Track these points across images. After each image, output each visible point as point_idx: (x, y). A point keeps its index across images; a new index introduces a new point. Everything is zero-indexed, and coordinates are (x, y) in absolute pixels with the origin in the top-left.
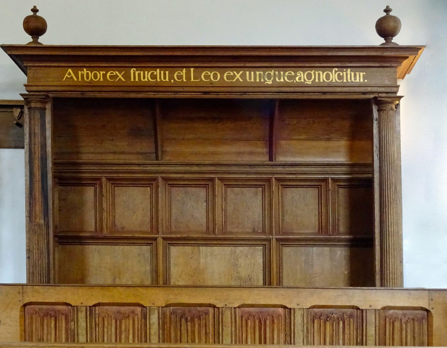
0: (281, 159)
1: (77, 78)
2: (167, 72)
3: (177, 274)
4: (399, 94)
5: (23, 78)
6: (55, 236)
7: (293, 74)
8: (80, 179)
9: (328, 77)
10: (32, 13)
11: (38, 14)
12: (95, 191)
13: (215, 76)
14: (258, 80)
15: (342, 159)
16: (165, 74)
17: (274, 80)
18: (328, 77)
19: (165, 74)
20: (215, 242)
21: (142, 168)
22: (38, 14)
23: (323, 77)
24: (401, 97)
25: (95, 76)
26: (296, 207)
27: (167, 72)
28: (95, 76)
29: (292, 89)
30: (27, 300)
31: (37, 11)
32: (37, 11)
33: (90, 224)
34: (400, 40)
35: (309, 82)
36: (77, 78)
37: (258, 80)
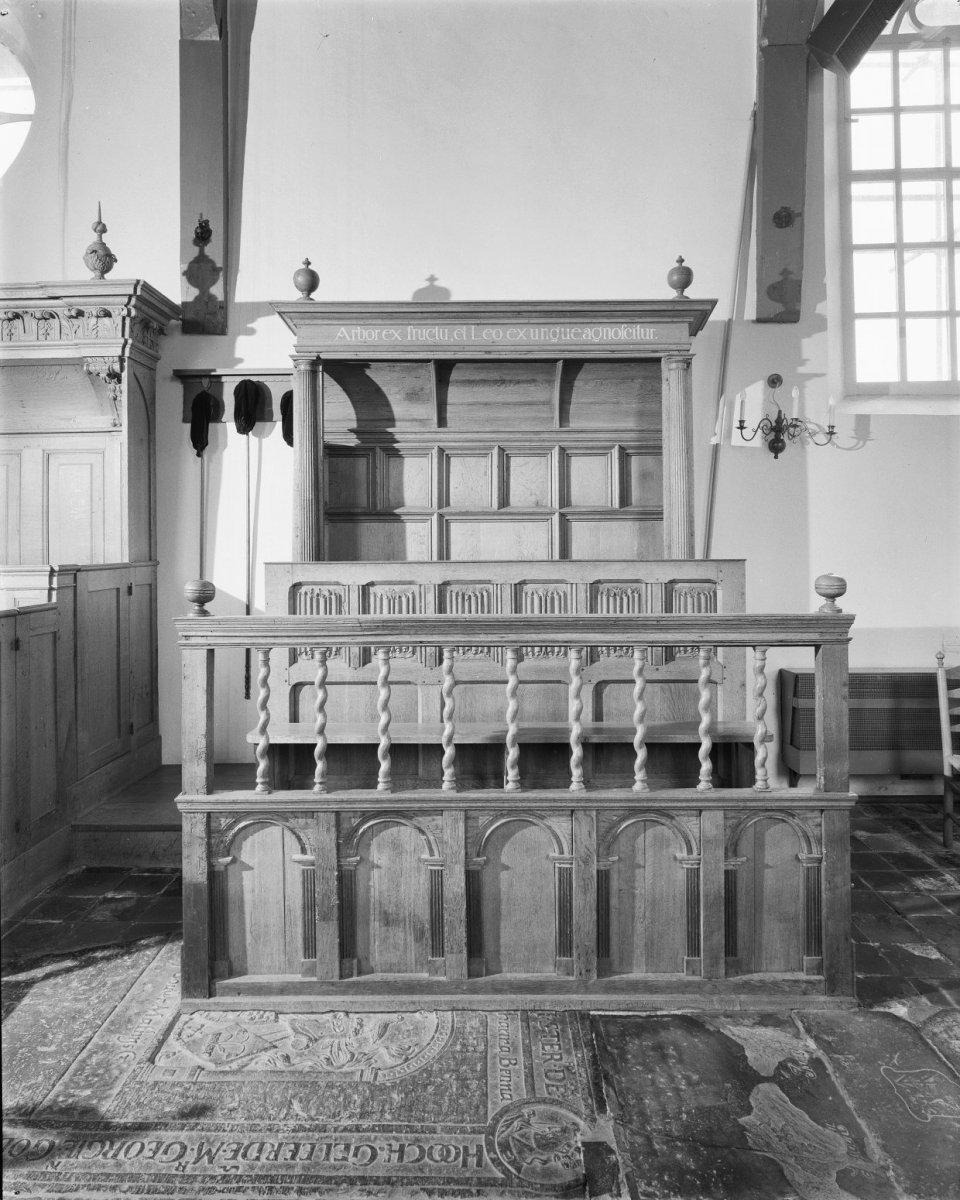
0: (573, 424)
1: (351, 337)
2: (446, 330)
3: (457, 551)
4: (849, 636)
5: (294, 340)
6: (325, 513)
7: (580, 331)
8: (398, 450)
9: (616, 334)
10: (304, 267)
11: (436, 283)
12: (368, 463)
13: (498, 334)
14: (543, 338)
15: (631, 424)
16: (444, 331)
17: (560, 338)
18: (616, 334)
19: (444, 331)
20: (266, 806)
21: (418, 436)
22: (436, 283)
23: (611, 334)
24: (850, 639)
25: (370, 335)
26: (262, 1118)
27: (446, 330)
28: (370, 335)
29: (578, 348)
30: (296, 581)
31: (436, 279)
32: (436, 279)
33: (363, 500)
34: (691, 293)
35: (596, 340)
36: (351, 337)
37: (543, 338)
